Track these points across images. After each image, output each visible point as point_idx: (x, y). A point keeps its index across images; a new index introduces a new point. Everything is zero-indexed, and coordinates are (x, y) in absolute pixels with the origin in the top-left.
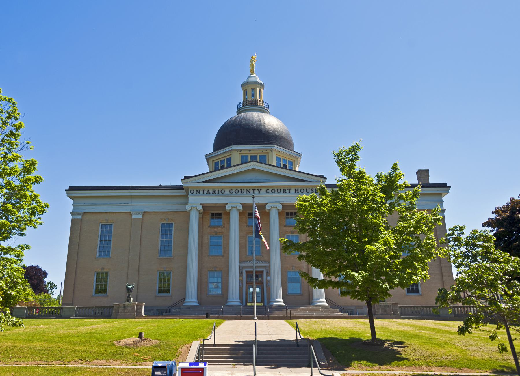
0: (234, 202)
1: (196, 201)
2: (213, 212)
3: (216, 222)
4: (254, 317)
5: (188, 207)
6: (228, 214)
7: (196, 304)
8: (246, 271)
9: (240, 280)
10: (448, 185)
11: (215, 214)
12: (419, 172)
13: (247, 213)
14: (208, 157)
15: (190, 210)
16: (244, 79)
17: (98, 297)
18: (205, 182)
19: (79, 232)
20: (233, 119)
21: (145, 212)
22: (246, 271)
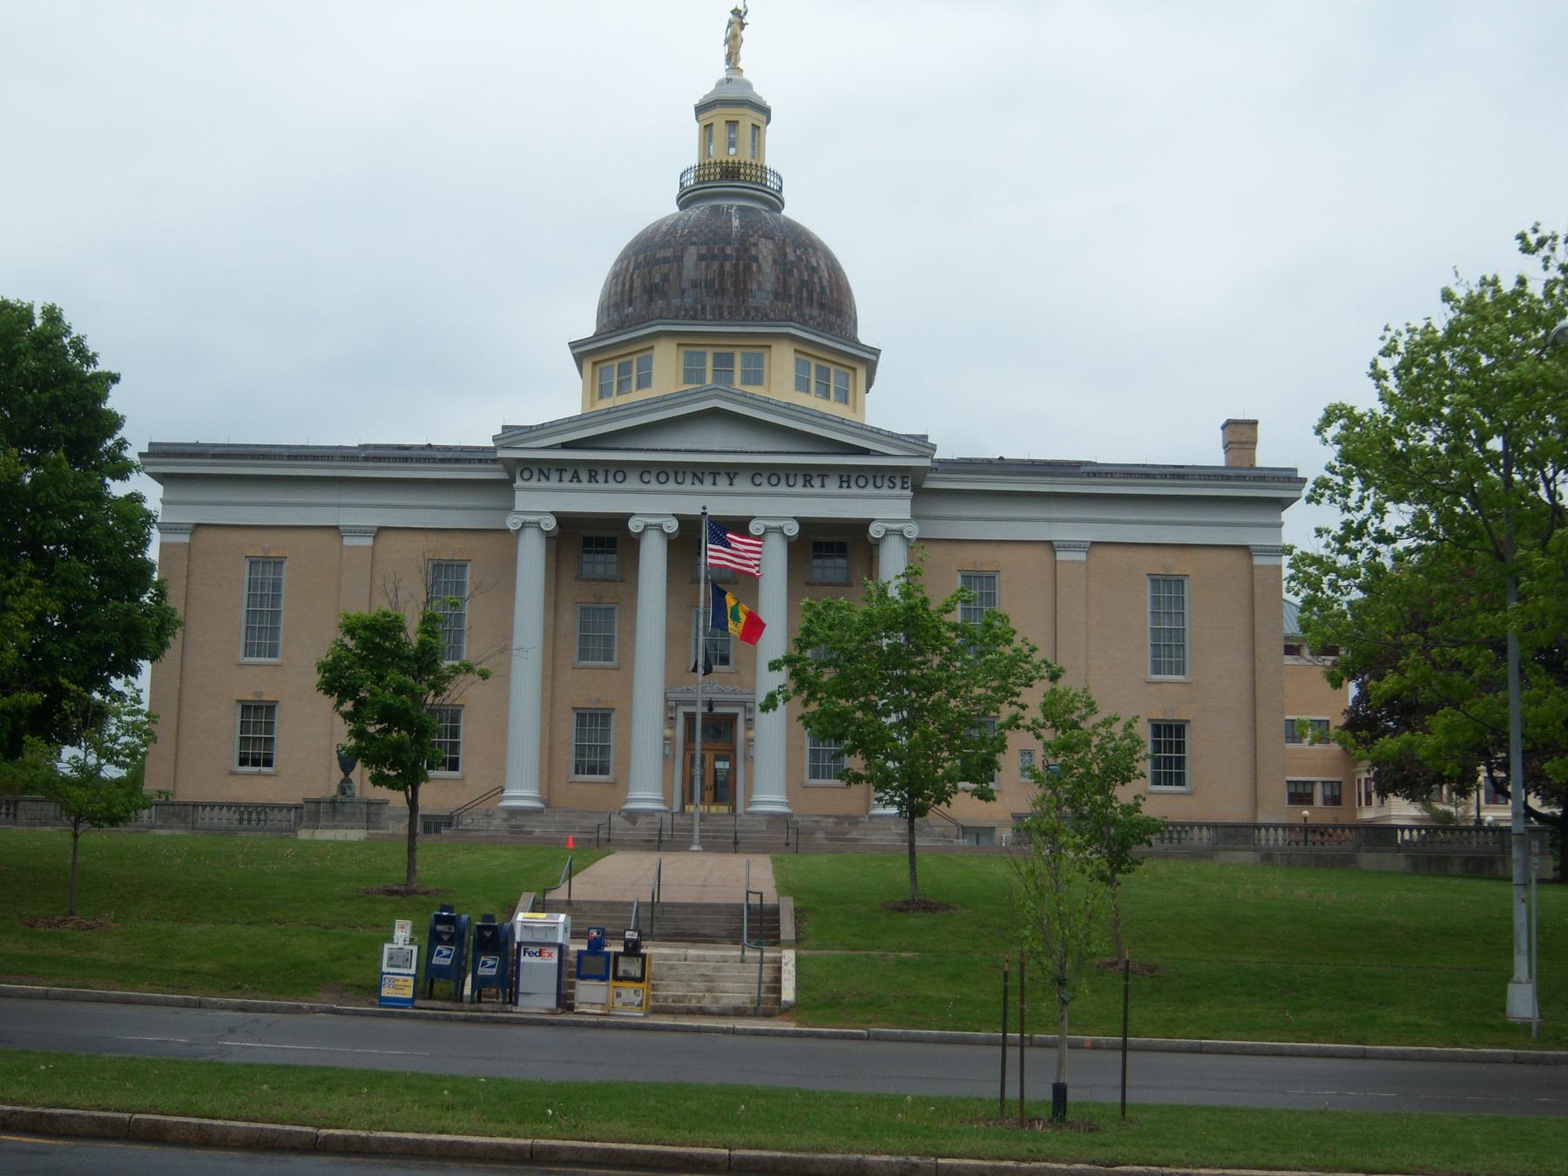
0: (652, 509)
1: (540, 503)
2: (590, 534)
3: (601, 564)
4: (692, 843)
5: (512, 522)
6: (634, 542)
7: (538, 805)
8: (736, 715)
9: (665, 738)
10: (1300, 475)
11: (592, 545)
12: (1230, 425)
13: (686, 539)
14: (583, 353)
15: (518, 531)
16: (704, 87)
17: (247, 774)
18: (566, 446)
19: (184, 582)
20: (664, 229)
21: (381, 529)
22: (736, 715)
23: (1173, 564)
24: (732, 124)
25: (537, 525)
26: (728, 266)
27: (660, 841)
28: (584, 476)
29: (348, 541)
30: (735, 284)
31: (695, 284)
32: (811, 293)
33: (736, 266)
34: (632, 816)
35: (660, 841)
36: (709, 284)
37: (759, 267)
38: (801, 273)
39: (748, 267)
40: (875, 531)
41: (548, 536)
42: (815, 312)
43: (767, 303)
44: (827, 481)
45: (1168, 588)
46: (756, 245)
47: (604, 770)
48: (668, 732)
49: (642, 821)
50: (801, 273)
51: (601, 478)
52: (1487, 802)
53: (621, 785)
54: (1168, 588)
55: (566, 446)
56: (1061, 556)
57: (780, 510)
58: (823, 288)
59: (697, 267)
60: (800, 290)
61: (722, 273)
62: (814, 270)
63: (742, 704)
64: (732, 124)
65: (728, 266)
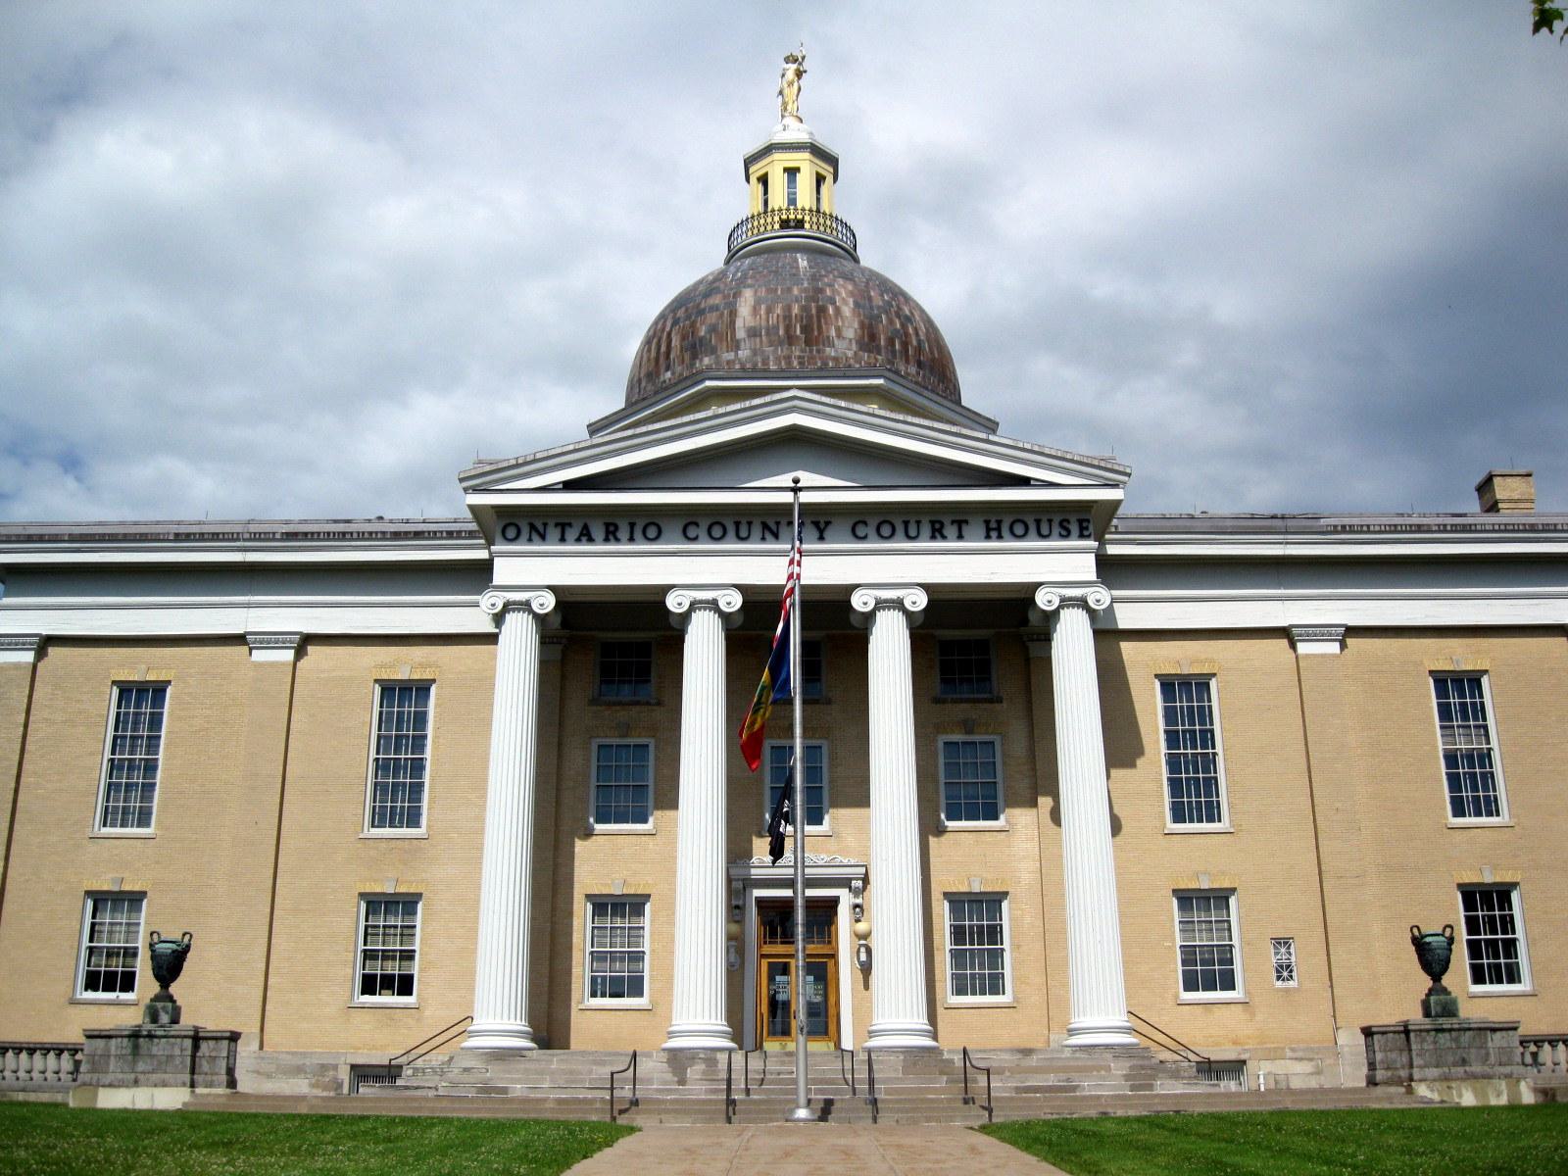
0: (702, 579)
1: (536, 572)
13: (752, 626)
18: (570, 486)
20: (711, 278)
23: (1460, 656)
24: (792, 172)
25: (526, 606)
26: (796, 310)
27: (731, 1103)
28: (598, 531)
29: (259, 656)
30: (806, 329)
31: (753, 333)
32: (905, 345)
33: (804, 309)
34: (679, 1060)
35: (731, 1103)
36: (771, 331)
37: (838, 310)
38: (891, 322)
39: (822, 310)
40: (1044, 600)
41: (541, 620)
42: (913, 370)
43: (850, 354)
44: (965, 529)
45: (1458, 693)
46: (831, 285)
47: (636, 988)
48: (734, 928)
49: (694, 1072)
50: (891, 322)
51: (623, 534)
52: (769, 1034)
53: (657, 1013)
54: (1458, 693)
55: (570, 486)
56: (1303, 648)
57: (890, 580)
58: (919, 341)
59: (755, 310)
60: (891, 342)
61: (787, 317)
62: (909, 319)
63: (844, 882)
64: (792, 172)
65: (796, 310)
